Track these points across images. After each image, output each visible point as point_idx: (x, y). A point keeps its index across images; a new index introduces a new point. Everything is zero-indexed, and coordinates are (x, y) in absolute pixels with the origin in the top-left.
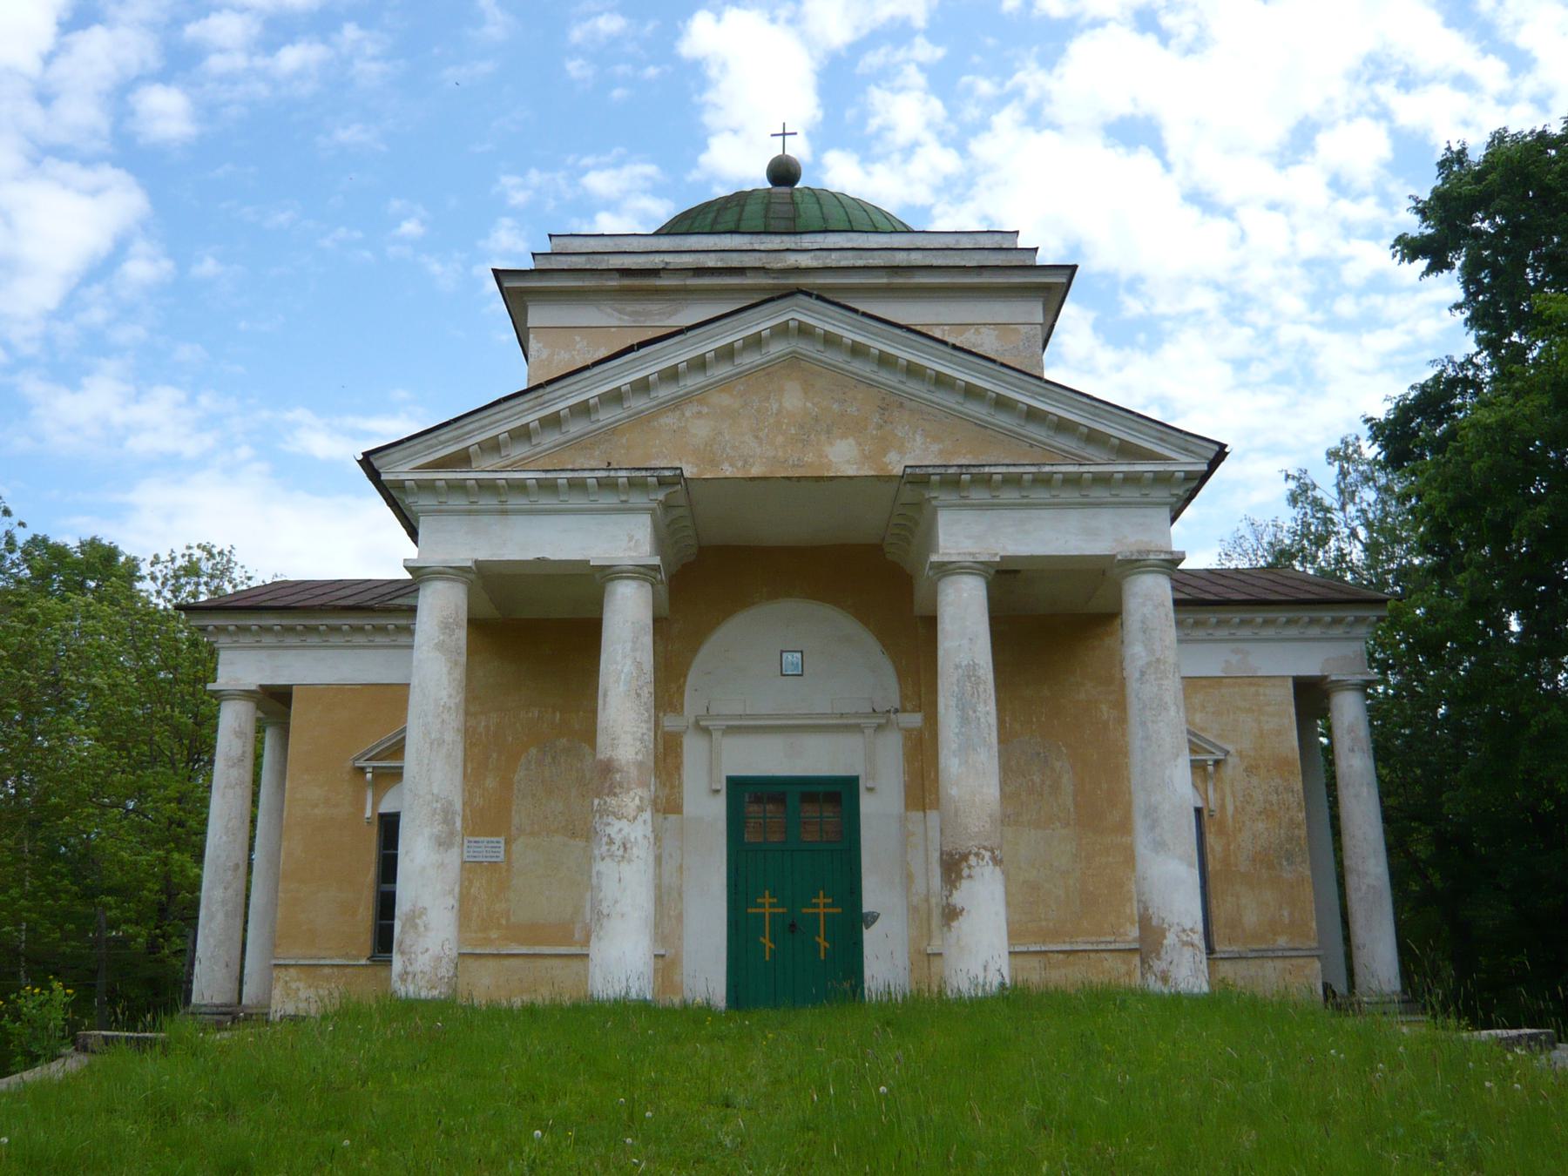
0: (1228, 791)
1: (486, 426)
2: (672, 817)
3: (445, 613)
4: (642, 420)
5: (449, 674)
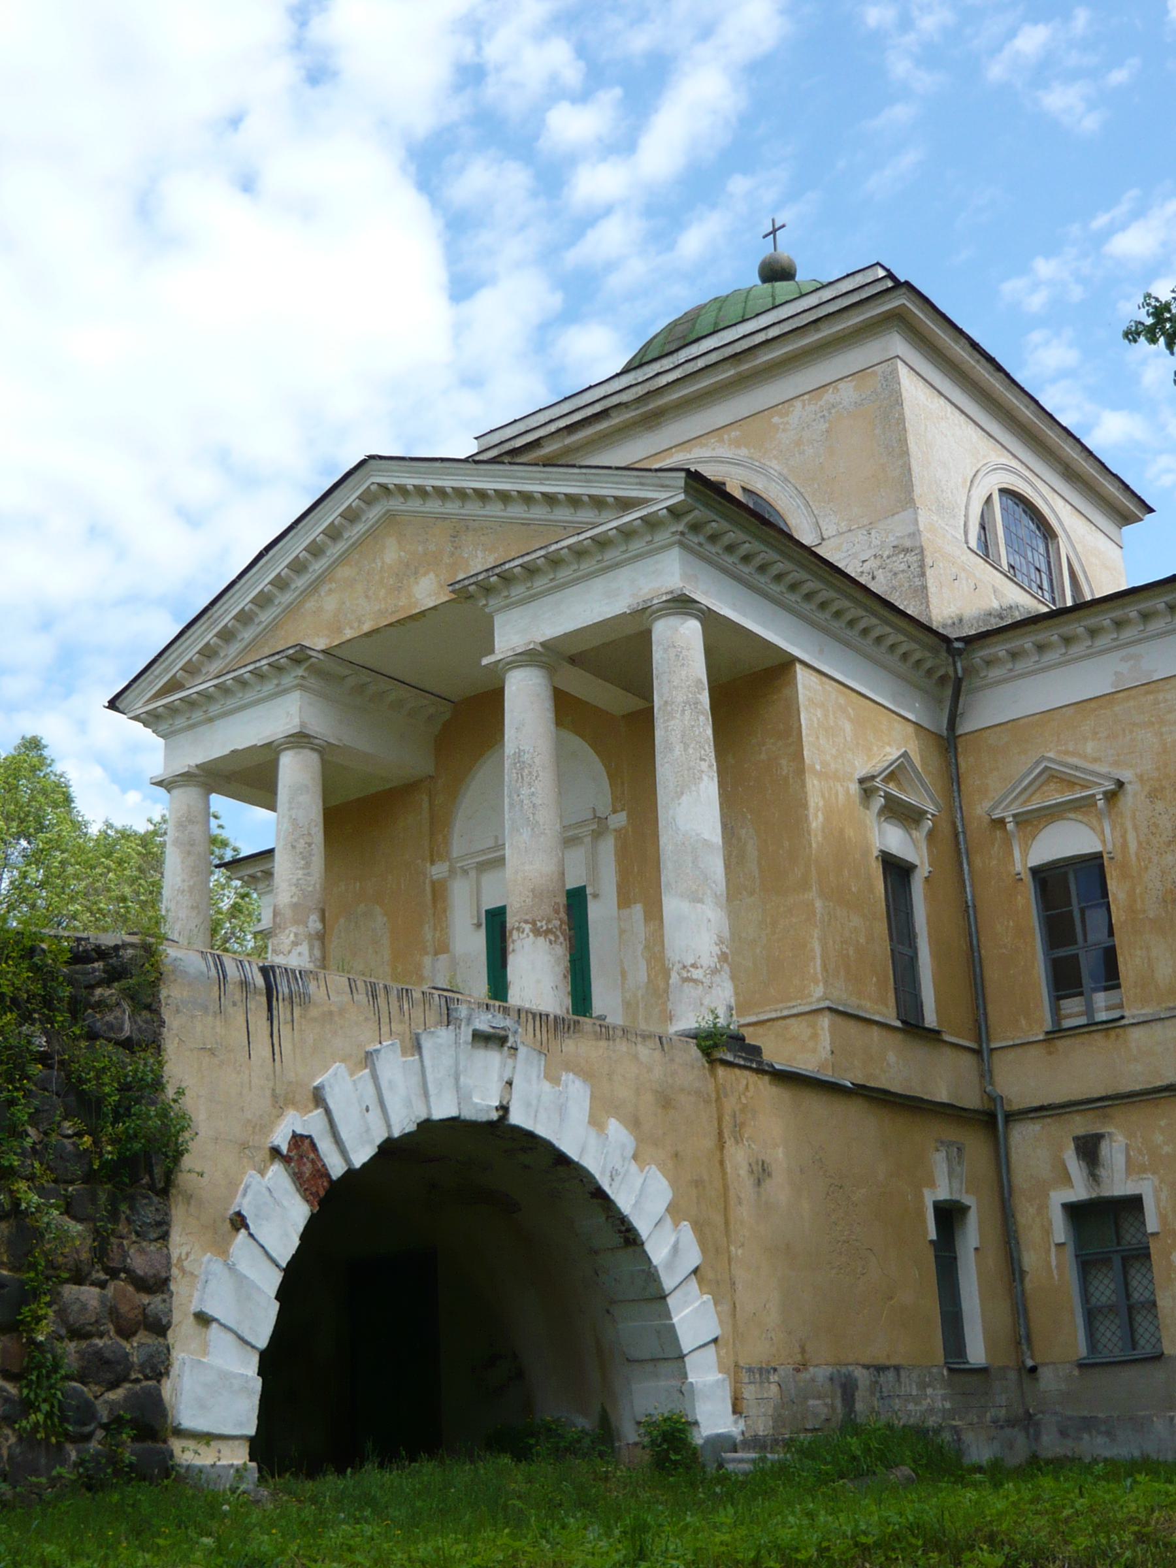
0: (1129, 825)
1: (183, 652)
2: (442, 957)
3: (179, 815)
4: (291, 610)
5: (183, 862)
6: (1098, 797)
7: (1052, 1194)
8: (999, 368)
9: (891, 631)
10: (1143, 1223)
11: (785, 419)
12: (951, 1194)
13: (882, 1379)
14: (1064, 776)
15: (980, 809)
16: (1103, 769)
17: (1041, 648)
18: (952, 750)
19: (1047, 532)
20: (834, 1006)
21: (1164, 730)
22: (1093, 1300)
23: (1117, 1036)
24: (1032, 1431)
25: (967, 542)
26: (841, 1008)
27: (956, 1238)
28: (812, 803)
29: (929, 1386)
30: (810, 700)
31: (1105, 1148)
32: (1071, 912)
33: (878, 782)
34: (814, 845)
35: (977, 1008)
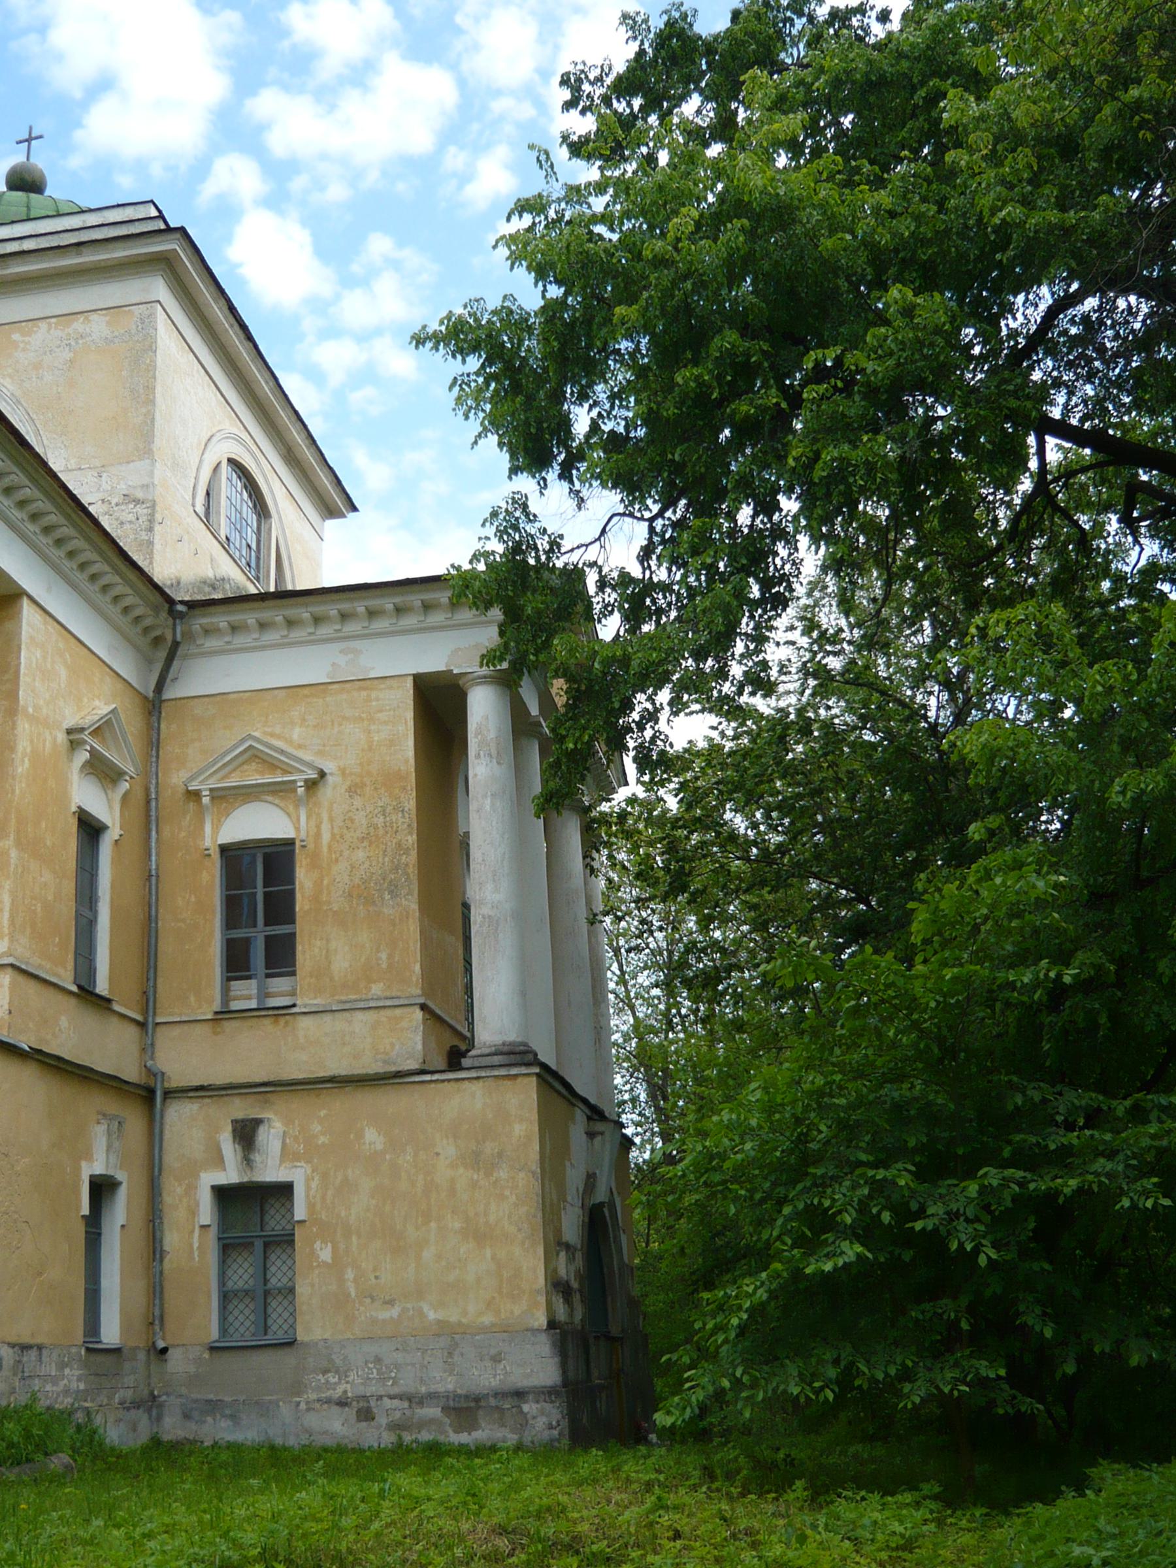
0: (325, 816)
6: (299, 784)
7: (203, 1175)
8: (250, 338)
9: (120, 581)
10: (291, 1210)
11: (27, 339)
12: (107, 1166)
13: (25, 1359)
14: (265, 757)
15: (177, 778)
16: (307, 757)
17: (263, 626)
18: (157, 714)
19: (261, 508)
20: (18, 964)
21: (372, 727)
22: (230, 1284)
23: (287, 1023)
24: (154, 1412)
25: (193, 506)
26: (23, 967)
27: (103, 1210)
28: (20, 748)
29: (67, 1366)
30: (32, 638)
31: (262, 1134)
32: (255, 894)
33: (85, 736)
34: (17, 792)
35: (148, 980)
